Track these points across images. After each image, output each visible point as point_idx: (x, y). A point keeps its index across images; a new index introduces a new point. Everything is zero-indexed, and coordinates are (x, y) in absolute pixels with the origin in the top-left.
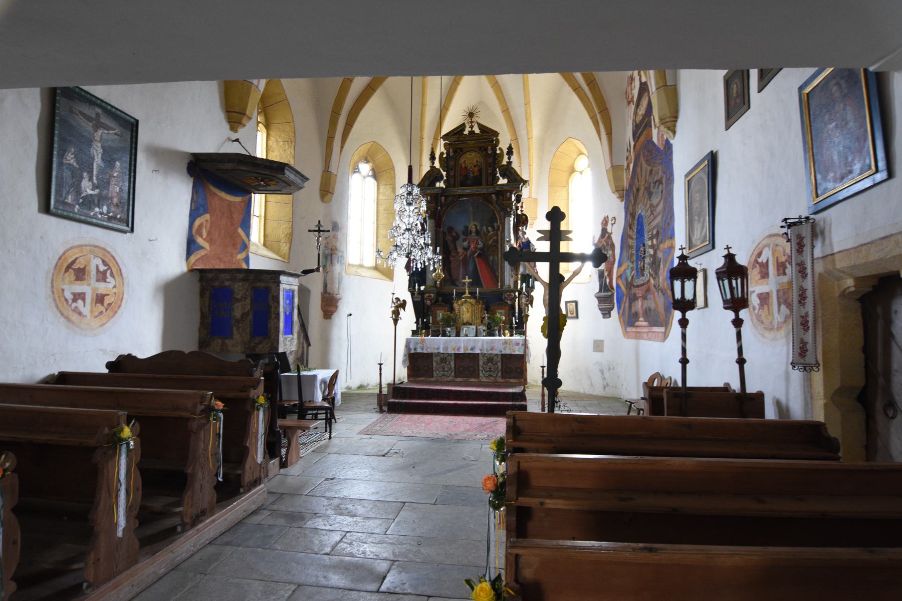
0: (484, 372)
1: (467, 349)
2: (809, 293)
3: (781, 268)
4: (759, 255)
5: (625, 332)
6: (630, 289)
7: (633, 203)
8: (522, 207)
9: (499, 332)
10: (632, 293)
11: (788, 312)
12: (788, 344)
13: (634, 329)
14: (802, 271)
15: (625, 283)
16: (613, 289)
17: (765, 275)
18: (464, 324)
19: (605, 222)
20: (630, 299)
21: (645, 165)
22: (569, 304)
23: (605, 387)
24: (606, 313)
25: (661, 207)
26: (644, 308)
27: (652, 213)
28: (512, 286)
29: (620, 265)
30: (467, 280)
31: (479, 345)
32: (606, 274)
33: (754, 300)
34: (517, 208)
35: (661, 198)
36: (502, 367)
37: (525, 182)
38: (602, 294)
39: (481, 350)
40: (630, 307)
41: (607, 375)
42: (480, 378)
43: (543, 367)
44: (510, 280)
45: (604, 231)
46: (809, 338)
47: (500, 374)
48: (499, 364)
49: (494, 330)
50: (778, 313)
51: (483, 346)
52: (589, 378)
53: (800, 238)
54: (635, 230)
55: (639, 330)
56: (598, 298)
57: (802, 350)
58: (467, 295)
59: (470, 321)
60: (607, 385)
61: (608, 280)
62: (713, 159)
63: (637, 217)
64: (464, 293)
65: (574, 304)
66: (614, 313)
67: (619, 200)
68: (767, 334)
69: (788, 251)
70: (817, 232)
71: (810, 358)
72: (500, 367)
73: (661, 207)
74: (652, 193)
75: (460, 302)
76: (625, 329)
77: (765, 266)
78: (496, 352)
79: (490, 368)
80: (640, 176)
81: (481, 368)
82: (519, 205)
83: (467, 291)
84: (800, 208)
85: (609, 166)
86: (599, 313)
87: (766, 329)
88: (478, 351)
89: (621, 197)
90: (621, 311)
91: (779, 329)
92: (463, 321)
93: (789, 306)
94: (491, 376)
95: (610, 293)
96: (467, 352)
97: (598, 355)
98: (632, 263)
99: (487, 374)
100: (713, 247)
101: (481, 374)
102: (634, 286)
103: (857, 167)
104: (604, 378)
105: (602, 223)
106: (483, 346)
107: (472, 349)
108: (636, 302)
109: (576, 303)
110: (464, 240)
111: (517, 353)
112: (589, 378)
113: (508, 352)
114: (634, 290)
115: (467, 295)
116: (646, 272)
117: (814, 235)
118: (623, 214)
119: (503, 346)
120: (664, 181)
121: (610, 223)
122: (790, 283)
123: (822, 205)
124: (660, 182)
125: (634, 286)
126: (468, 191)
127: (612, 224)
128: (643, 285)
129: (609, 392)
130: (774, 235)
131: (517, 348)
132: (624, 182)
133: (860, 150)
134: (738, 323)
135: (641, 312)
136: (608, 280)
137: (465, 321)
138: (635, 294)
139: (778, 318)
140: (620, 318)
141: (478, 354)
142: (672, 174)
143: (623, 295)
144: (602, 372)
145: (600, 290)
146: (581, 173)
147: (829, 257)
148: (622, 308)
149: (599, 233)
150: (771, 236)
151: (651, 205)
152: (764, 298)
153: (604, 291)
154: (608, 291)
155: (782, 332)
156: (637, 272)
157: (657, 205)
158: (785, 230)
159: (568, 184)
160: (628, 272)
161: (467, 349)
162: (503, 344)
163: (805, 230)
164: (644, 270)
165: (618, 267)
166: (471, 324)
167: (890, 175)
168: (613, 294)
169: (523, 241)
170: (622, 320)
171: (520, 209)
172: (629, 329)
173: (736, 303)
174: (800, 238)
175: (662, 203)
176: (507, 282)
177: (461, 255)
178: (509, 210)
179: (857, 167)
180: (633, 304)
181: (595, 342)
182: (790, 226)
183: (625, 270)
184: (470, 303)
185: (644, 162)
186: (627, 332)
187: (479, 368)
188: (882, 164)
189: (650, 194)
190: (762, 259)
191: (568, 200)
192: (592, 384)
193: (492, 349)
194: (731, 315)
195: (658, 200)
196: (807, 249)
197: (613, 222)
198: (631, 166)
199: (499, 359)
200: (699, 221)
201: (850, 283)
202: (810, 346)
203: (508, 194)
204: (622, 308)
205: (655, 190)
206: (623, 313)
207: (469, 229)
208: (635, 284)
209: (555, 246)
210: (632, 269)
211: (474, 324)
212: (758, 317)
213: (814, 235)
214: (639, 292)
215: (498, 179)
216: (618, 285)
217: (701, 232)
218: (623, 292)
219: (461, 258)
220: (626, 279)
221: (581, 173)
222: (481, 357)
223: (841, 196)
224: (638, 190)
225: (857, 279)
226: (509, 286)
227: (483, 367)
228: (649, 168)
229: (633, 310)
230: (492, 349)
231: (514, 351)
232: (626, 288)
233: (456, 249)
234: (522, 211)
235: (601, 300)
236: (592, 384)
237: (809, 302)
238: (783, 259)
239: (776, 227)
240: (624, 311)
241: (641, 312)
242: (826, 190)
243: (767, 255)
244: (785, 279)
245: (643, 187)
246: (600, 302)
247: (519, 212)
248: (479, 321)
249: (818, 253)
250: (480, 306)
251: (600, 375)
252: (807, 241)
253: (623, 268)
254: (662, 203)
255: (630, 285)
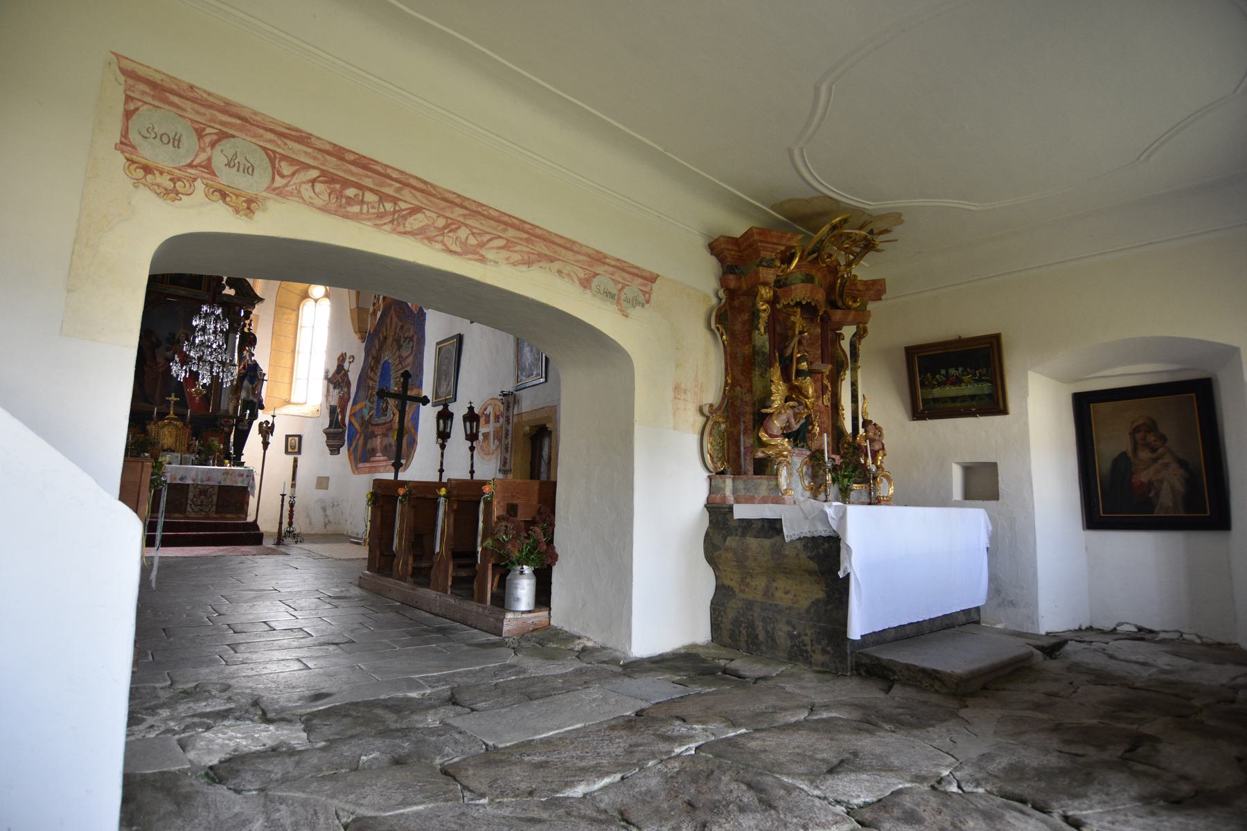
0: (193, 506)
1: (175, 479)
2: (510, 432)
3: (497, 418)
4: (486, 409)
5: (354, 468)
6: (367, 427)
7: (377, 347)
8: (250, 325)
9: (214, 461)
10: (370, 431)
11: (498, 443)
12: (497, 461)
13: (368, 465)
14: (508, 421)
15: (360, 421)
16: (345, 426)
17: (487, 422)
18: (164, 451)
19: (342, 358)
20: (365, 436)
21: (395, 320)
22: (290, 439)
23: (326, 525)
24: (334, 450)
25: (410, 360)
26: (384, 443)
27: (400, 363)
28: (231, 411)
29: (355, 403)
30: (173, 398)
31: (193, 474)
32: (339, 410)
33: (481, 437)
34: (245, 325)
35: (411, 354)
36: (218, 500)
37: (261, 300)
38: (332, 430)
39: (194, 481)
40: (365, 443)
41: (329, 512)
42: (187, 513)
43: (283, 495)
44: (229, 404)
45: (340, 368)
46: (508, 456)
47: (214, 509)
48: (215, 498)
49: (209, 459)
50: (493, 445)
51: (197, 476)
52: (308, 516)
53: (508, 403)
54: (379, 374)
55: (374, 465)
56: (326, 434)
57: (504, 463)
58: (172, 415)
59: (173, 447)
60: (329, 522)
61: (340, 417)
62: (460, 338)
63: (382, 362)
64: (168, 414)
65: (297, 439)
66: (344, 450)
67: (360, 341)
68: (485, 457)
69: (502, 409)
70: (516, 401)
71: (508, 467)
72: (215, 500)
73: (410, 360)
74: (402, 346)
75: (160, 423)
76: (356, 466)
77: (488, 416)
78: (213, 483)
79: (202, 502)
80: (388, 327)
81: (189, 502)
82: (247, 322)
83: (172, 412)
84: (509, 387)
85: (354, 306)
86: (327, 450)
87: (485, 454)
88: (189, 481)
89: (362, 339)
90: (352, 449)
91: (493, 454)
92: (162, 446)
93: (500, 441)
94: (201, 510)
95: (341, 430)
96: (174, 482)
97: (321, 493)
98: (372, 403)
99: (196, 509)
100: (455, 401)
101: (189, 509)
102: (372, 425)
103: (535, 373)
104: (326, 516)
105: (339, 359)
106: (197, 476)
107: (182, 479)
108: (374, 439)
109: (300, 437)
110: (168, 350)
111: (239, 485)
112: (308, 516)
113: (228, 483)
114: (371, 428)
115: (172, 415)
116: (389, 413)
117: (515, 402)
118: (363, 355)
119: (223, 477)
120: (415, 339)
121: (347, 360)
122: (502, 427)
123: (520, 387)
124: (411, 339)
125: (372, 425)
126: (184, 293)
127: (350, 363)
128: (385, 423)
129: (330, 529)
130: (496, 399)
131: (240, 479)
132: (367, 324)
133: (537, 366)
134: (472, 449)
135: (379, 448)
136: (340, 417)
137: (165, 447)
138: (373, 432)
139: (493, 447)
140: (349, 455)
141: (188, 485)
142: (423, 336)
143: (357, 432)
144: (324, 509)
145: (330, 426)
146: (316, 301)
147: (520, 414)
148: (354, 445)
149: (335, 368)
150: (492, 399)
151: (400, 356)
152: (486, 436)
153: (335, 428)
154: (340, 427)
155: (494, 456)
156: (377, 412)
157: (407, 357)
158: (501, 397)
159: (299, 309)
160: (365, 411)
161: (175, 479)
162: (223, 474)
163: (511, 399)
164: (386, 410)
165: (353, 405)
166: (174, 451)
167: (546, 381)
168: (343, 432)
169: (250, 363)
170: (352, 457)
171: (248, 327)
172: (361, 465)
173: (472, 437)
174: (508, 403)
175: (411, 357)
176: (223, 406)
177: (162, 366)
178: (236, 325)
179: (535, 373)
180: (369, 442)
181: (319, 478)
182: (504, 395)
183: (361, 409)
184: (177, 426)
185: (394, 316)
186: (357, 468)
187: (186, 502)
188: (544, 375)
189: (400, 347)
190: (487, 412)
191: (297, 325)
192: (311, 523)
193: (209, 480)
194: (469, 444)
195: (407, 354)
196: (511, 409)
197: (351, 360)
198: (379, 314)
199: (216, 490)
200: (445, 380)
201: (527, 428)
202: (508, 461)
203: (237, 308)
204: (354, 445)
205: (404, 344)
206: (354, 450)
207: (177, 336)
208: (374, 423)
209: (405, 386)
210: (371, 409)
211: (178, 452)
212: (481, 447)
213: (515, 402)
214: (378, 431)
215: (224, 288)
216: (350, 422)
217: (447, 388)
218: (356, 429)
219: (161, 370)
220: (362, 418)
221: (316, 301)
222: (191, 488)
223: (528, 385)
224: (385, 338)
225: (531, 427)
226: (227, 411)
227: (192, 501)
228: (400, 324)
229: (369, 446)
230: (209, 480)
231: (236, 483)
232: (361, 426)
233: (155, 358)
234: (249, 329)
235: (329, 435)
236: (311, 523)
237: (510, 437)
238: (498, 413)
239: (497, 395)
240: (357, 446)
241: (379, 448)
242: (522, 380)
243: (489, 410)
244: (498, 425)
245: (391, 338)
246: (328, 438)
247: (246, 330)
248: (184, 448)
249: (515, 412)
250: (188, 430)
251: (322, 512)
252: (511, 405)
253: (358, 407)
254: (411, 357)
255: (366, 424)
